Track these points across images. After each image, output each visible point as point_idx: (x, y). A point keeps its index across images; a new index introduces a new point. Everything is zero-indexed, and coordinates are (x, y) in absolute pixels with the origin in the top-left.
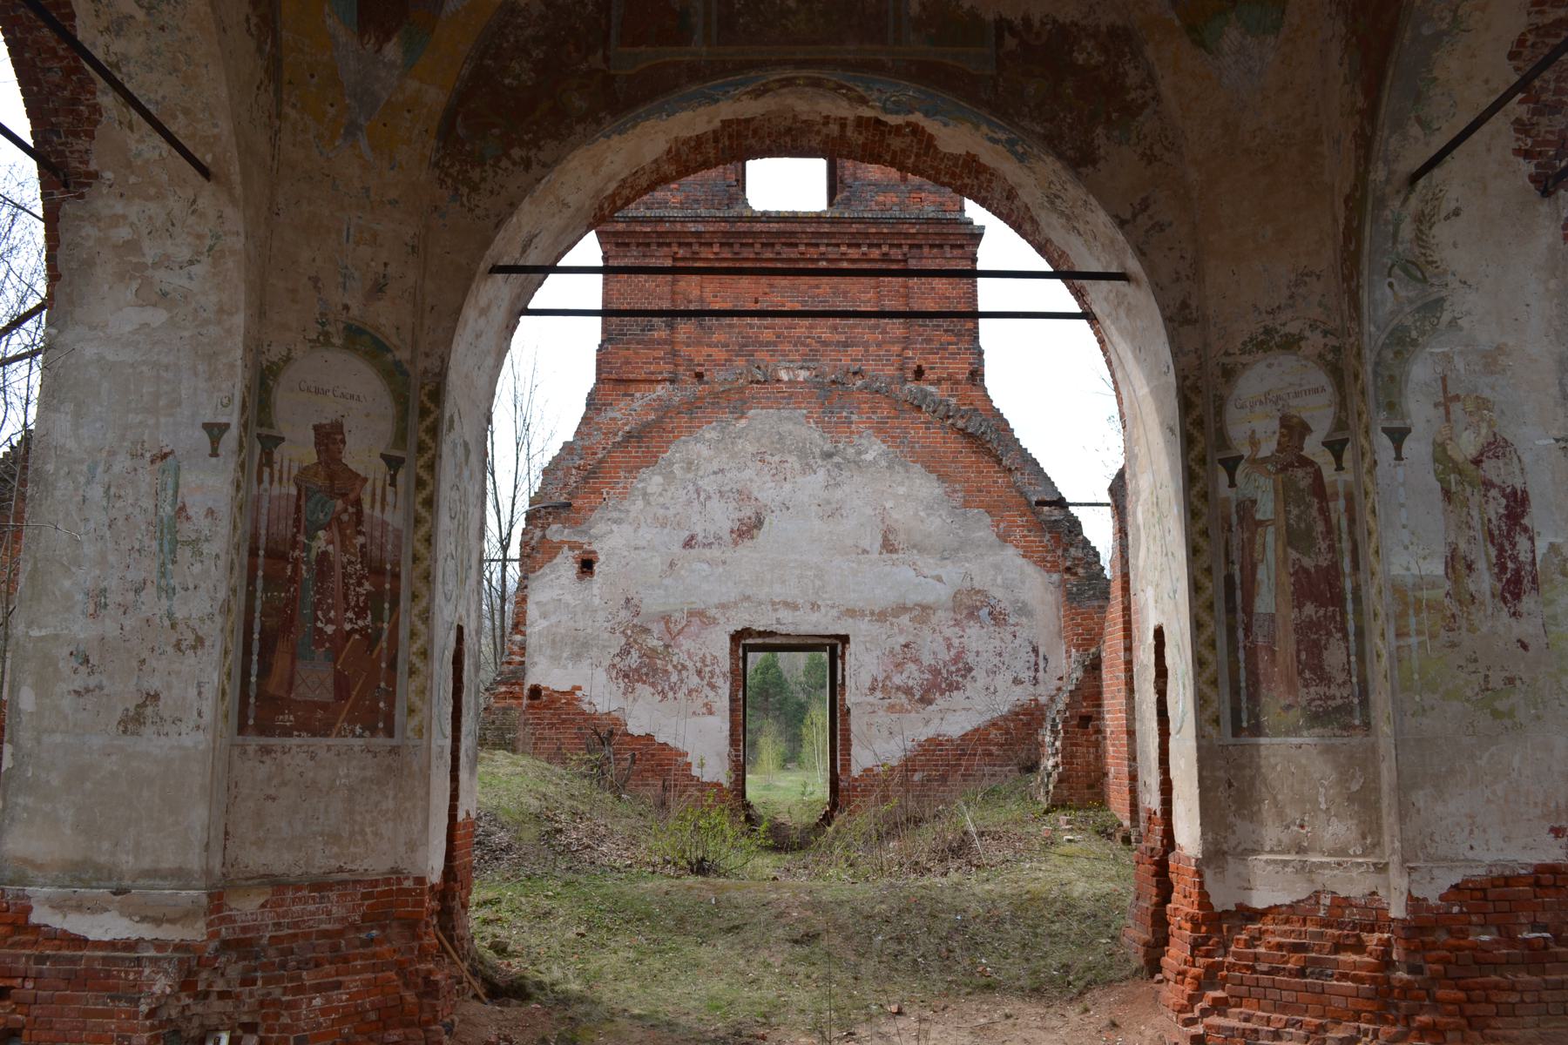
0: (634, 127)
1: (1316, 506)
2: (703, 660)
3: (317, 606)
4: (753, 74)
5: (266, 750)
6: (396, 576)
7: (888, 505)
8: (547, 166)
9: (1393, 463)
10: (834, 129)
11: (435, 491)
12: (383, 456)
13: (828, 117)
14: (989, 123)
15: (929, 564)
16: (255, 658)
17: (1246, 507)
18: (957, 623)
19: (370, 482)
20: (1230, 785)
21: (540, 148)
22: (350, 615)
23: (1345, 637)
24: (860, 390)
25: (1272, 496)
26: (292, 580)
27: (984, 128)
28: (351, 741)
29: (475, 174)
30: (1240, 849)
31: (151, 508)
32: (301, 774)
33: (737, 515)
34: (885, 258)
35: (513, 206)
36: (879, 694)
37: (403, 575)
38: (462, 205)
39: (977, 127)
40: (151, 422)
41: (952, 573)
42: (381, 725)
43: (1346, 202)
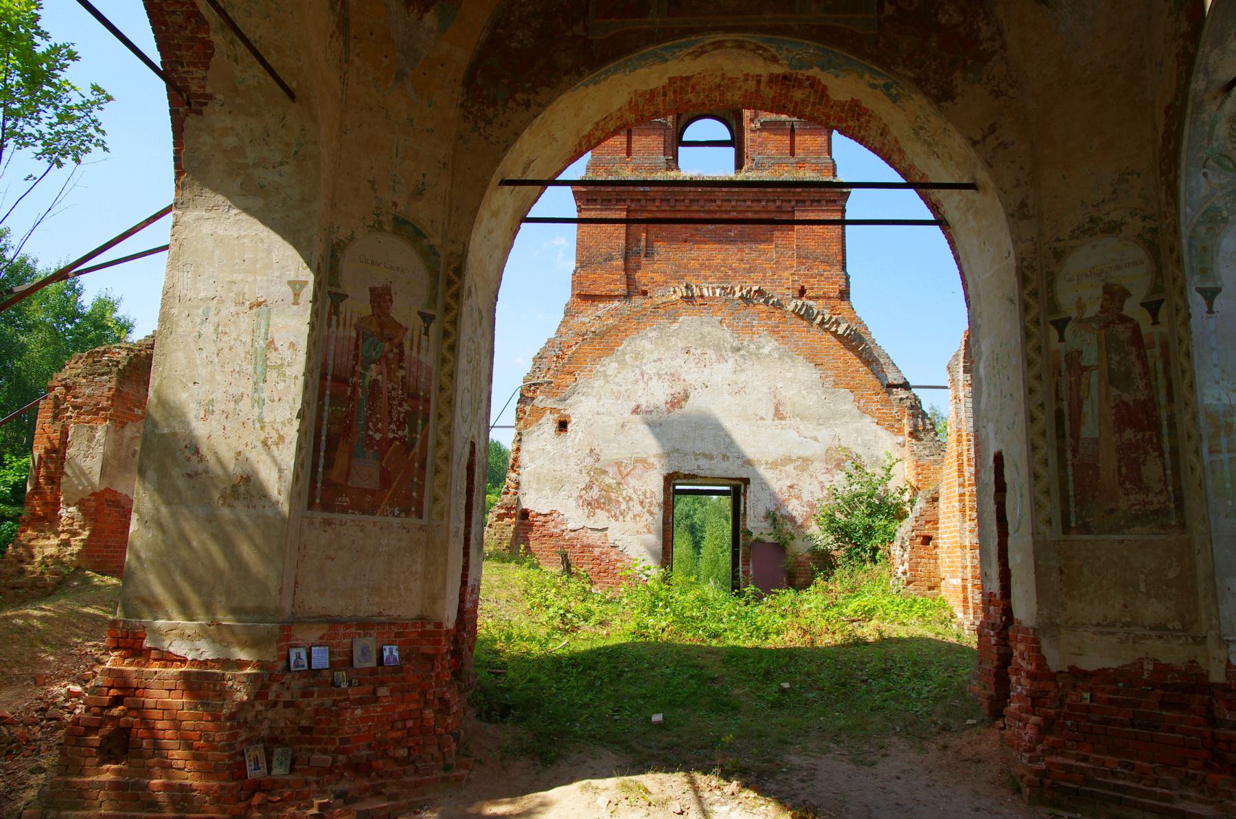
0: (605, 79)
1: (1135, 353)
2: (645, 494)
3: (368, 419)
4: (693, 38)
5: (328, 523)
6: (427, 401)
8: (542, 106)
9: (1205, 315)
10: (752, 85)
11: (458, 340)
12: (419, 313)
13: (747, 75)
14: (872, 71)
15: (809, 429)
16: (322, 454)
17: (1073, 359)
18: (828, 471)
19: (409, 332)
20: (1061, 572)
21: (537, 93)
22: (393, 427)
23: (1161, 455)
26: (351, 399)
27: (867, 76)
28: (390, 519)
29: (490, 112)
31: (249, 341)
32: (354, 542)
33: (670, 391)
34: (779, 210)
35: (517, 135)
37: (432, 400)
38: (480, 134)
39: (861, 76)
40: (250, 279)
41: (825, 434)
42: (413, 509)
43: (1166, 112)
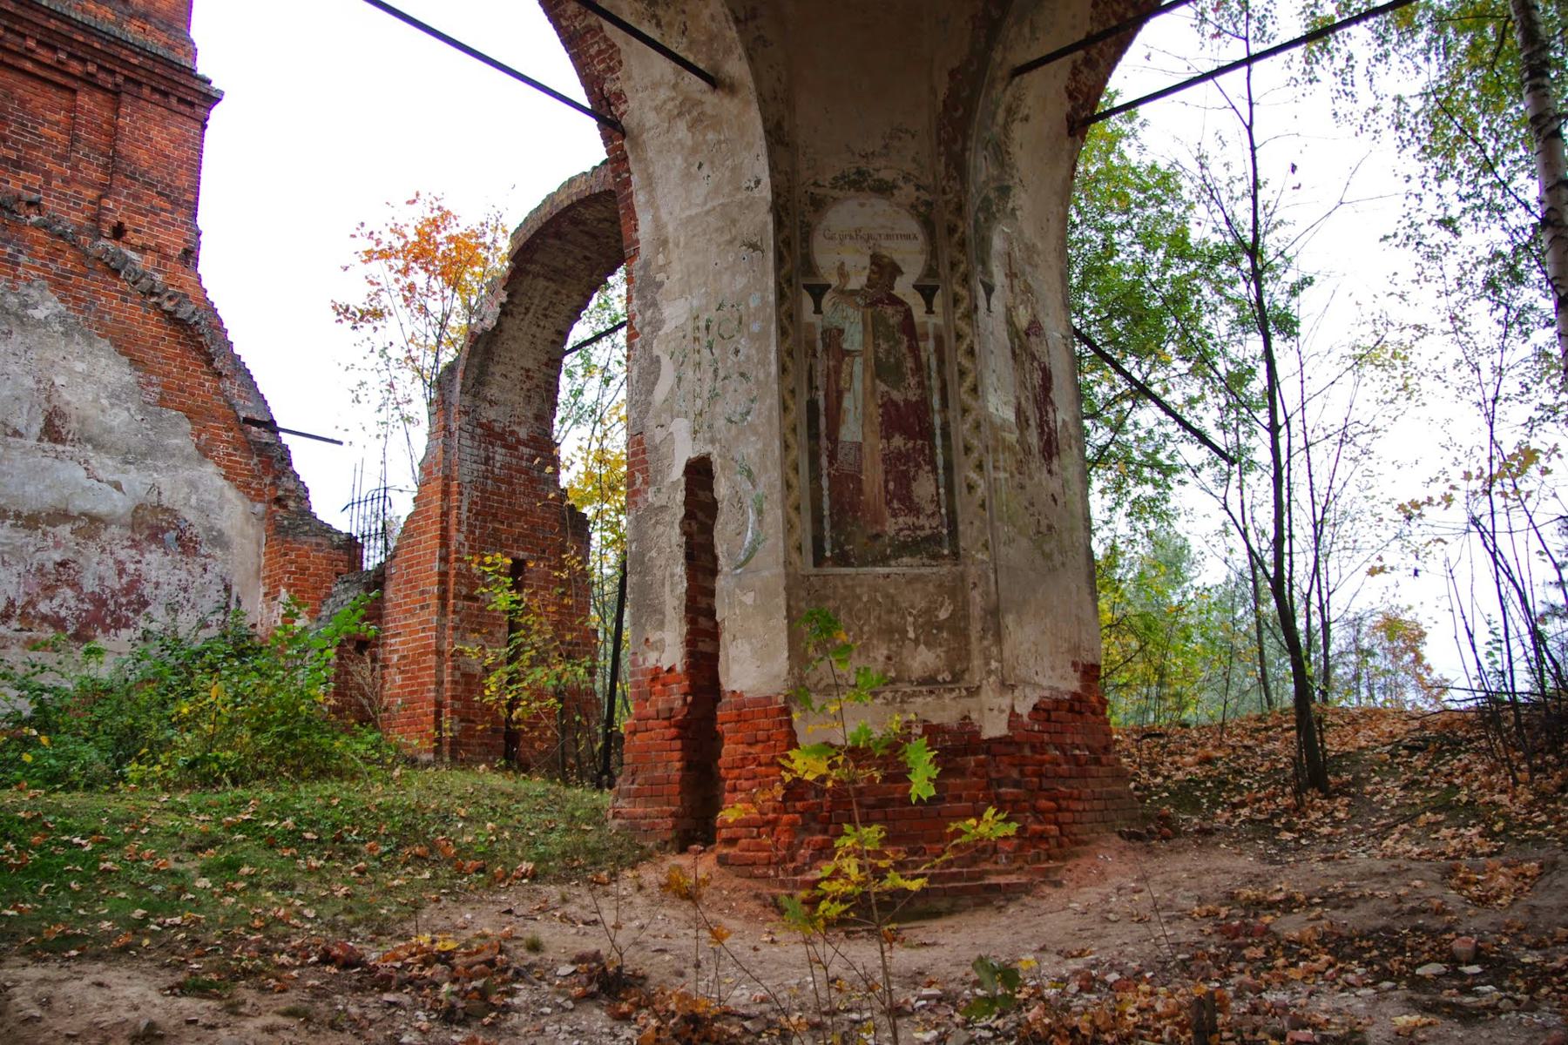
1: (906, 343)
7: (59, 381)
15: (106, 466)
17: (833, 336)
18: (135, 545)
23: (934, 470)
24: (36, 226)
25: (860, 327)
30: (821, 686)
36: (15, 624)
41: (137, 481)
